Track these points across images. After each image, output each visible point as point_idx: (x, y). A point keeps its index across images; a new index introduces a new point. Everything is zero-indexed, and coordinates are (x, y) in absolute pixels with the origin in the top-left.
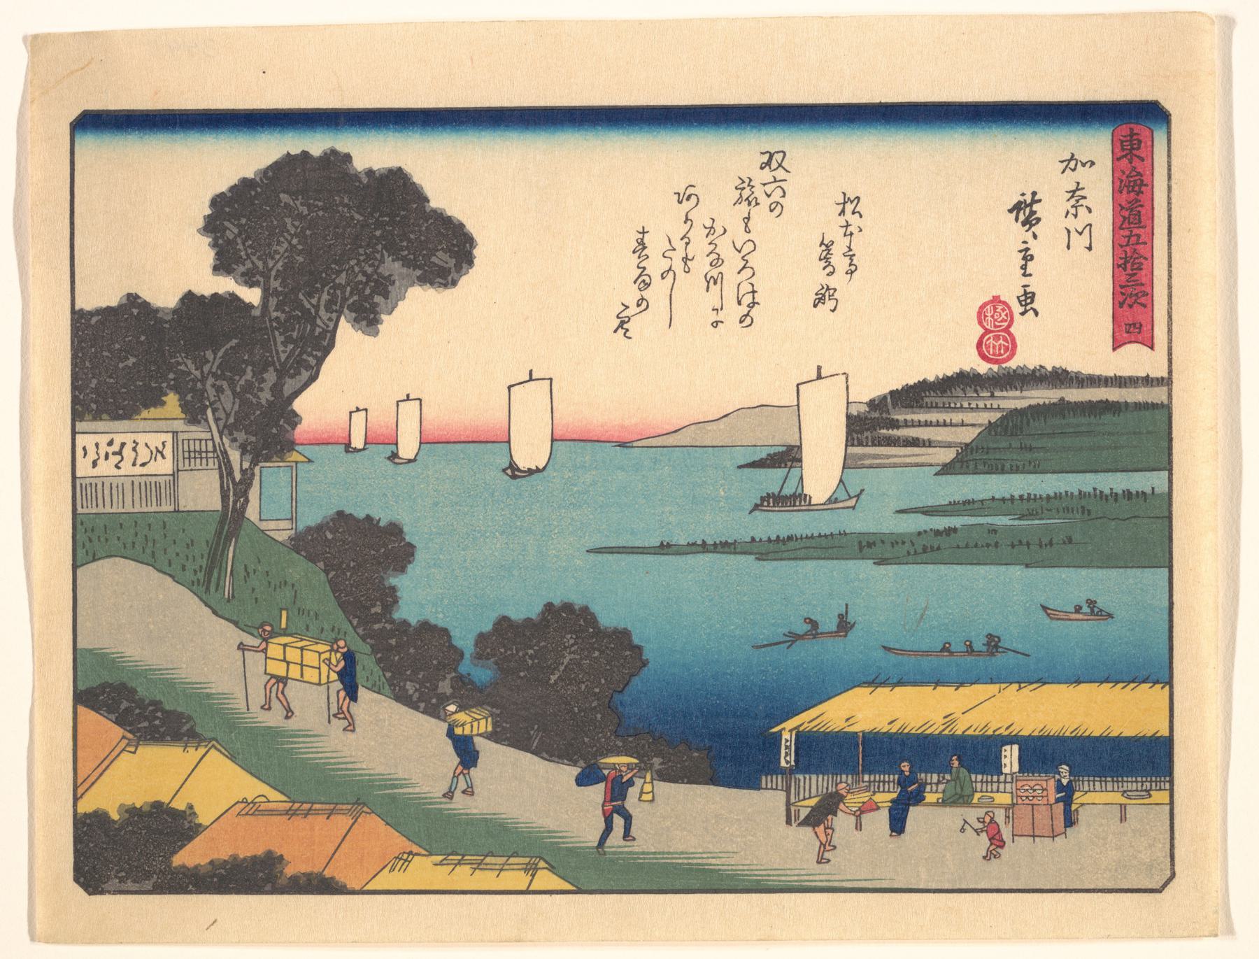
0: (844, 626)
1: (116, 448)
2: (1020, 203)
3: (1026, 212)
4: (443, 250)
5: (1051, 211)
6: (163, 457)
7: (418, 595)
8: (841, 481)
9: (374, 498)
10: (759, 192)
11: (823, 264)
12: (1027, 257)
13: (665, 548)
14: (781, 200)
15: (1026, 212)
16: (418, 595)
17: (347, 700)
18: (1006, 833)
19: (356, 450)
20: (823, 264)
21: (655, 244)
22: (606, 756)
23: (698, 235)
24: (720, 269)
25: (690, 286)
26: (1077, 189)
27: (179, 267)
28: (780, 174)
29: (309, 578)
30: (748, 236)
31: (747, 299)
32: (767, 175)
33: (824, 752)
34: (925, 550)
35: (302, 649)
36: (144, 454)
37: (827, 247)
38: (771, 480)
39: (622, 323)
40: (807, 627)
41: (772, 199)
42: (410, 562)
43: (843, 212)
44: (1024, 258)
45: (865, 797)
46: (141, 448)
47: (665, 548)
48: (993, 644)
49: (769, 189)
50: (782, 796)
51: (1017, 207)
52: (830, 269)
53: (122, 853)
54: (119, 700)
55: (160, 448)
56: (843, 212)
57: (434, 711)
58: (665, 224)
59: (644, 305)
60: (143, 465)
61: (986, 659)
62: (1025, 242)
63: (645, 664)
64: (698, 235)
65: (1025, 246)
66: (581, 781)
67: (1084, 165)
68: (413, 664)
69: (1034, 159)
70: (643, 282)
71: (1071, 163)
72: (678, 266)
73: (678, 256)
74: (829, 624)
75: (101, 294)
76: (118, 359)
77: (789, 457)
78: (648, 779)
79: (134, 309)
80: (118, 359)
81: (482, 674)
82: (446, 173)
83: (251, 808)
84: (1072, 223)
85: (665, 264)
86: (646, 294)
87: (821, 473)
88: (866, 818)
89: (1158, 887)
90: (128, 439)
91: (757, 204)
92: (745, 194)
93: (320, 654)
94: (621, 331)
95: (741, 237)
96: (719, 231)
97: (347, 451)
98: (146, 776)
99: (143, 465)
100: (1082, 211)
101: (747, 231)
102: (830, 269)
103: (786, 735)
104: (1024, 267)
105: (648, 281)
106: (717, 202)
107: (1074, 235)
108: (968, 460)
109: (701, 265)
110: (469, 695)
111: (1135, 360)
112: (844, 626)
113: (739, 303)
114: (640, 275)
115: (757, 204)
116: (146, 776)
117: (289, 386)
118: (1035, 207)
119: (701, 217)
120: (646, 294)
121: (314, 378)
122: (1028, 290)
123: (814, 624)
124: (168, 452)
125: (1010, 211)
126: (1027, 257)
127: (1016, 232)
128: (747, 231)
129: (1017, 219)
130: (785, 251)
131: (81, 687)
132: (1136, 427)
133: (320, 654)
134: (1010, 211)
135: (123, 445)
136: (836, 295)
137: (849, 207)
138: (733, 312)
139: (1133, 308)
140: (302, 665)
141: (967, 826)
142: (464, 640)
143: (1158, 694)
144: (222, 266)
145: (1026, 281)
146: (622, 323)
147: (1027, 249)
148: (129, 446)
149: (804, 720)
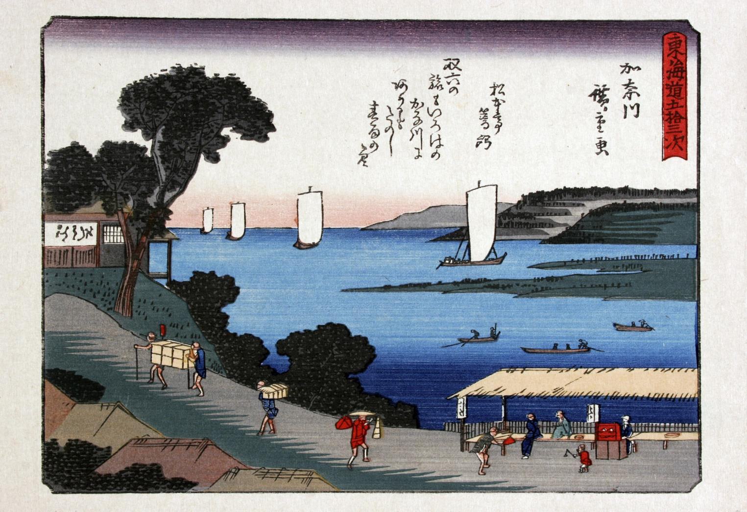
0: (494, 336)
1: (62, 231)
2: (596, 90)
3: (600, 95)
4: (257, 122)
5: (615, 95)
6: (91, 235)
7: (241, 318)
8: (493, 248)
9: (216, 259)
10: (443, 82)
11: (482, 122)
12: (601, 120)
13: (387, 288)
14: (457, 86)
15: (600, 95)
16: (241, 318)
17: (200, 378)
18: (592, 457)
19: (206, 233)
20: (482, 122)
21: (382, 112)
22: (352, 411)
23: (407, 106)
24: (420, 126)
25: (402, 137)
26: (630, 83)
27: (100, 125)
28: (456, 71)
29: (180, 306)
30: (437, 107)
31: (437, 143)
32: (448, 72)
33: (484, 409)
34: (542, 290)
35: (173, 347)
36: (80, 234)
37: (484, 111)
38: (452, 248)
39: (363, 159)
40: (473, 335)
41: (452, 85)
42: (213, 273)
43: (494, 93)
44: (599, 122)
45: (506, 436)
46: (78, 230)
47: (387, 288)
48: (584, 347)
49: (449, 80)
50: (457, 436)
51: (594, 94)
52: (486, 125)
53: (69, 466)
54: (69, 379)
55: (89, 230)
56: (494, 93)
57: (254, 387)
58: (388, 98)
59: (375, 147)
60: (79, 240)
61: (582, 355)
62: (600, 113)
63: (375, 356)
64: (407, 106)
65: (599, 115)
66: (339, 427)
67: (633, 69)
68: (245, 359)
69: (602, 67)
70: (375, 134)
71: (627, 68)
72: (395, 126)
73: (394, 119)
74: (485, 333)
75: (58, 142)
76: (71, 179)
77: (462, 235)
78: (378, 425)
79: (76, 151)
80: (71, 179)
81: (281, 362)
82: (260, 71)
83: (140, 441)
84: (628, 103)
85: (388, 124)
86: (377, 140)
87: (482, 240)
88: (508, 448)
89: (689, 490)
90: (71, 225)
91: (442, 89)
92: (435, 84)
93: (184, 351)
94: (362, 163)
95: (433, 107)
96: (420, 105)
97: (201, 233)
98: (88, 423)
99: (79, 240)
100: (634, 96)
101: (436, 103)
102: (486, 125)
103: (460, 400)
104: (600, 127)
105: (377, 133)
106: (419, 90)
107: (629, 109)
108: (571, 236)
109: (408, 124)
110: (273, 376)
111: (675, 175)
112: (494, 336)
113: (431, 144)
114: (373, 130)
115: (442, 89)
116: (88, 423)
117: (168, 196)
118: (605, 93)
119: (409, 97)
120: (377, 140)
121: (181, 192)
122: (602, 140)
123: (477, 334)
124: (94, 232)
125: (590, 96)
126: (601, 120)
127: (597, 107)
128: (436, 103)
129: (595, 100)
130: (459, 119)
131: (46, 368)
132: (679, 213)
133: (184, 351)
134: (590, 96)
135: (68, 228)
136: (490, 140)
137: (498, 90)
138: (428, 150)
139: (675, 143)
140: (161, 355)
141: (568, 454)
142: (270, 343)
143: (692, 374)
144: (130, 126)
145: (600, 135)
146: (363, 159)
147: (601, 117)
148: (71, 229)
149: (472, 389)
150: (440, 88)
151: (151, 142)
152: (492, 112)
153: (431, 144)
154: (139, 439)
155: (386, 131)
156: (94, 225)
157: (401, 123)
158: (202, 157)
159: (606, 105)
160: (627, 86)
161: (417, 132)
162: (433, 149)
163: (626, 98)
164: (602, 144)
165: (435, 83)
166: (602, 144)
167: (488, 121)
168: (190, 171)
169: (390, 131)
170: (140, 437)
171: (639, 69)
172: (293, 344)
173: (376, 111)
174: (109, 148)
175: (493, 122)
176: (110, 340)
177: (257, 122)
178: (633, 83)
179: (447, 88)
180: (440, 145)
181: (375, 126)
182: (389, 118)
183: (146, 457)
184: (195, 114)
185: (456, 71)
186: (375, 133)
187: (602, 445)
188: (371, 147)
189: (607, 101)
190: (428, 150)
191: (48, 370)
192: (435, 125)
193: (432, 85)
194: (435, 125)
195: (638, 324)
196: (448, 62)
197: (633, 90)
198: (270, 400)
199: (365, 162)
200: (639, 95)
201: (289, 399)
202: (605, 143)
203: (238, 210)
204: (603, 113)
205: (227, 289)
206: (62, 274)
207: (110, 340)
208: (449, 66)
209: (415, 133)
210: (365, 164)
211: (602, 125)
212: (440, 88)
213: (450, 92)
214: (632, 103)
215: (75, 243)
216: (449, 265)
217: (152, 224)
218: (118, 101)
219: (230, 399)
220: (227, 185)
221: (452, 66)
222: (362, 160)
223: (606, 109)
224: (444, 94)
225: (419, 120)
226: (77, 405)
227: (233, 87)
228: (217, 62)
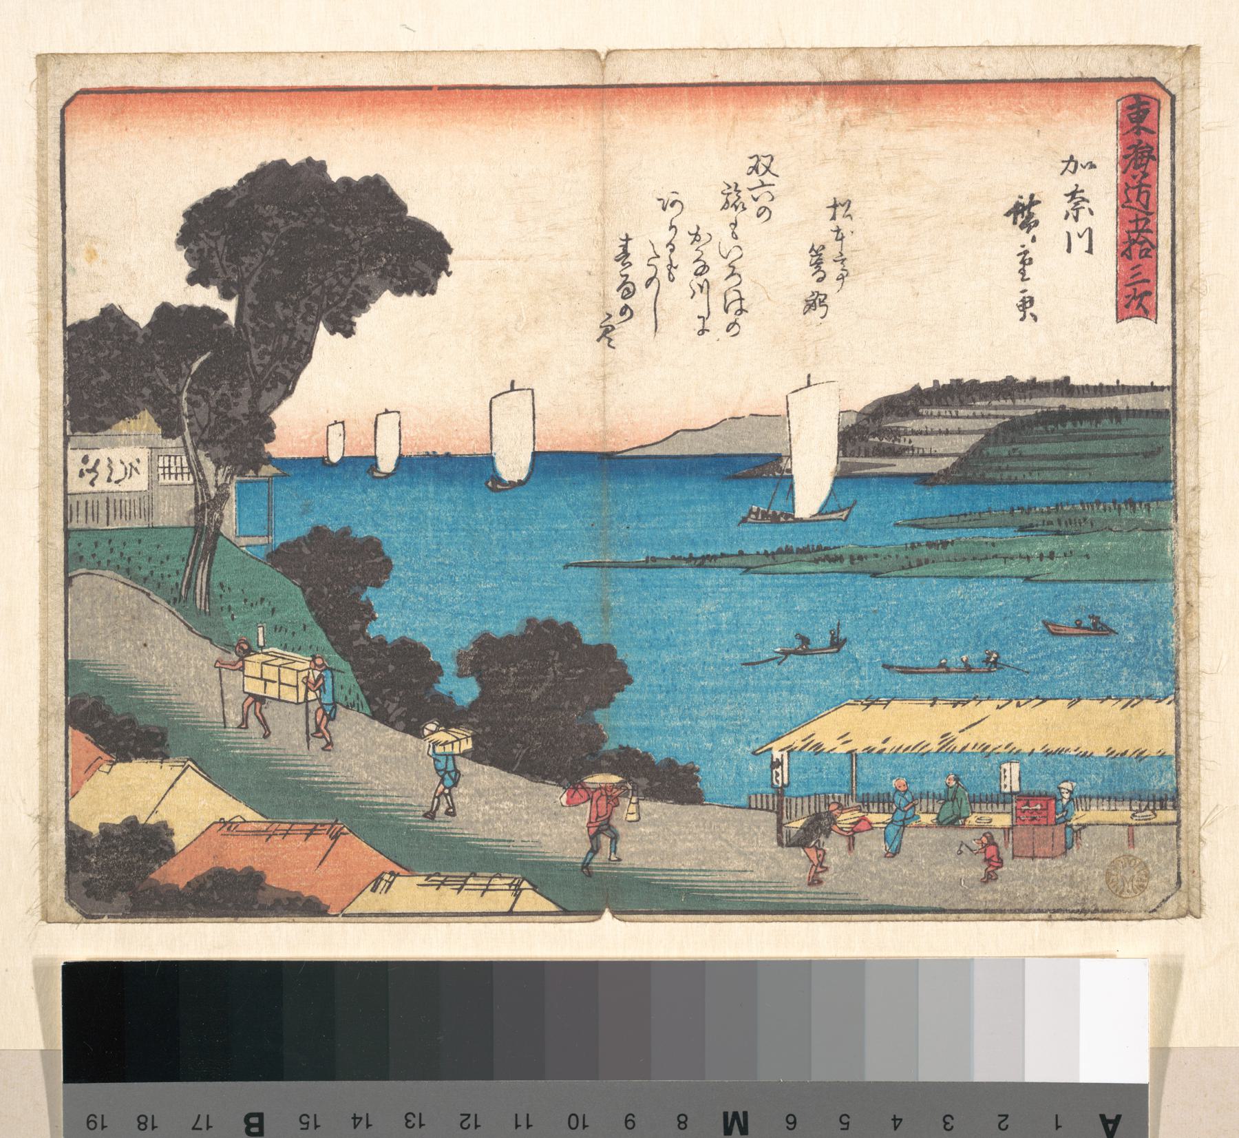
1: (91, 465)
3: (1023, 213)
4: (416, 258)
5: (1051, 214)
7: (392, 616)
10: (745, 195)
12: (1025, 260)
14: (771, 206)
15: (1023, 213)
16: (392, 616)
22: (589, 773)
23: (683, 240)
27: (150, 277)
28: (768, 178)
30: (736, 242)
31: (737, 305)
32: (754, 180)
39: (607, 332)
43: (834, 218)
49: (756, 193)
52: (821, 275)
56: (834, 218)
64: (683, 240)
65: (1022, 250)
70: (627, 289)
73: (662, 264)
76: (107, 370)
79: (112, 319)
80: (107, 370)
81: (465, 691)
83: (227, 826)
85: (650, 272)
91: (744, 209)
92: (732, 199)
95: (728, 243)
99: (117, 482)
105: (631, 289)
109: (685, 272)
110: (450, 716)
123: (805, 640)
126: (1025, 260)
129: (1015, 223)
134: (1007, 215)
145: (1023, 286)
146: (607, 332)
147: (1026, 252)
150: (740, 208)
151: (234, 302)
152: (832, 250)
153: (726, 311)
154: (225, 823)
155: (647, 286)
156: (143, 454)
157: (673, 270)
158: (322, 331)
159: (1034, 231)
160: (1073, 195)
161: (702, 287)
162: (731, 317)
163: (1071, 217)
164: (1026, 303)
165: (732, 199)
166: (1026, 303)
167: (823, 267)
168: (301, 354)
169: (654, 285)
170: (227, 819)
171: (1093, 166)
172: (485, 656)
173: (629, 250)
174: (164, 312)
175: (832, 269)
176: (170, 660)
177: (416, 258)
178: (1082, 191)
179: (753, 208)
180: (742, 310)
181: (627, 276)
182: (652, 262)
183: (240, 855)
184: (312, 247)
185: (768, 178)
186: (627, 289)
187: (1022, 833)
188: (622, 313)
189: (1037, 223)
190: (719, 320)
191: (74, 326)
192: (732, 274)
193: (727, 202)
194: (732, 274)
195: (1087, 622)
196: (753, 162)
197: (1082, 204)
198: (447, 755)
199: (610, 340)
200: (1092, 213)
201: (475, 756)
202: (1032, 300)
203: (388, 423)
204: (1029, 245)
205: (371, 561)
206: (90, 546)
207: (170, 660)
208: (755, 168)
209: (698, 289)
210: (612, 344)
211: (1027, 268)
212: (740, 208)
213: (759, 216)
214: (1080, 227)
215: (112, 487)
216: (757, 522)
217: (239, 438)
218: (180, 250)
219: (381, 760)
220: (367, 384)
221: (762, 169)
222: (604, 335)
223: (1034, 240)
224: (748, 219)
225: (705, 266)
226: (118, 765)
227: (375, 195)
228: (348, 152)
